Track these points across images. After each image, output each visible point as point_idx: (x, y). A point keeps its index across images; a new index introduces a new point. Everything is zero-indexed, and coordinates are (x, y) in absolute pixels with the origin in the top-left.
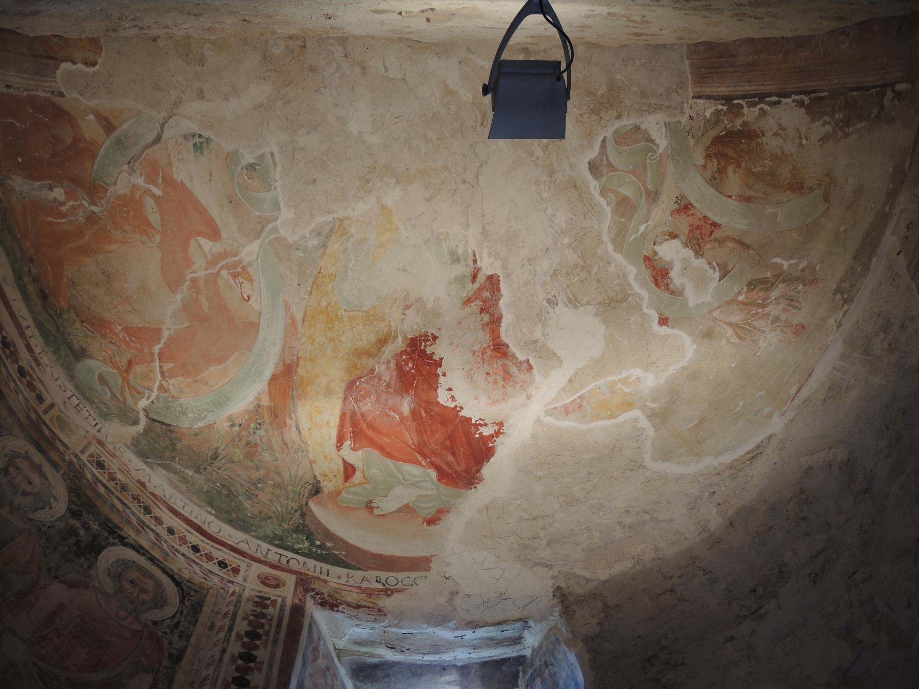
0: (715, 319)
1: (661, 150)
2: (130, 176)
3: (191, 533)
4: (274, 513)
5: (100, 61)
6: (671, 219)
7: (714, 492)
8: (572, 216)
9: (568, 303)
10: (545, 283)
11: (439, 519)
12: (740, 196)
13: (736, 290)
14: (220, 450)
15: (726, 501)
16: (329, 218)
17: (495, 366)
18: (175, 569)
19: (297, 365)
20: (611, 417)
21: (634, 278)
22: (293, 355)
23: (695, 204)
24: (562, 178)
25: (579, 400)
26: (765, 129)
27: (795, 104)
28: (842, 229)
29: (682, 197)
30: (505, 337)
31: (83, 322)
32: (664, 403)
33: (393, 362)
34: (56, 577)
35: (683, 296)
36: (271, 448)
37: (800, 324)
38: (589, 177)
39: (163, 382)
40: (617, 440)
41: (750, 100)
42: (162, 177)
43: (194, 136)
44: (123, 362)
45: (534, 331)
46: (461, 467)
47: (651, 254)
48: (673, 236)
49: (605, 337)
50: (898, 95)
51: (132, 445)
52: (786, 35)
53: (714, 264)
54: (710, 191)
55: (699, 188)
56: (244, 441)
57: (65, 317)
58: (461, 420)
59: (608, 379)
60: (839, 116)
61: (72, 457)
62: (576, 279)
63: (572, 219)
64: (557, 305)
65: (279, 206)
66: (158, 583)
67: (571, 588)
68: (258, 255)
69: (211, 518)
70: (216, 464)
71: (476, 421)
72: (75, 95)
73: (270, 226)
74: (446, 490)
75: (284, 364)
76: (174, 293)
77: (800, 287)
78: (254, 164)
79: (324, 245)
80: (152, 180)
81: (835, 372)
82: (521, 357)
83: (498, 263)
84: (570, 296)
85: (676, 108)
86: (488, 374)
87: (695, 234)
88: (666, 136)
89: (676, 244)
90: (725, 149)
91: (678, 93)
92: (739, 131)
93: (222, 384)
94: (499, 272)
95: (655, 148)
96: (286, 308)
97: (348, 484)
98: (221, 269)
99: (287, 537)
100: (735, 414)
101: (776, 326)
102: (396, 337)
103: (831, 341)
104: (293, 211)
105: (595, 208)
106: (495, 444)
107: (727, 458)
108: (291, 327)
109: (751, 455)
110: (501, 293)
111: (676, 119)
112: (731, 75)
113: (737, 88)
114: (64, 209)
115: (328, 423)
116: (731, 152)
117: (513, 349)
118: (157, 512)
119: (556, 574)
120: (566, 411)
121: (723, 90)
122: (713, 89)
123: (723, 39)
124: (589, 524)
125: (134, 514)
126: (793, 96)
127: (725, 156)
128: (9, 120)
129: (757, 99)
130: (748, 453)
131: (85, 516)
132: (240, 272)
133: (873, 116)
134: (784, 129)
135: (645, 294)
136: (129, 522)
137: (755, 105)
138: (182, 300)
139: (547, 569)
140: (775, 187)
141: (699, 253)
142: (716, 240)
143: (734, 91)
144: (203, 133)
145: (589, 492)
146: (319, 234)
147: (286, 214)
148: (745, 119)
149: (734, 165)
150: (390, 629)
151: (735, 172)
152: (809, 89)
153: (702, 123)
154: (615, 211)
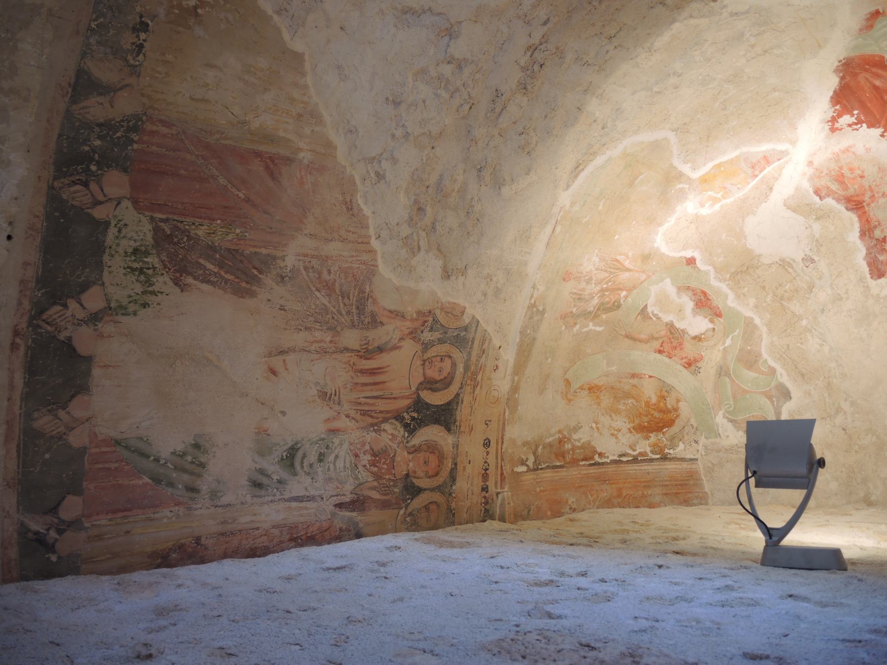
0: (643, 272)
1: (721, 413)
6: (702, 353)
7: (603, 128)
8: (802, 346)
9: (792, 262)
10: (820, 278)
11: (868, 20)
12: (642, 378)
13: (630, 299)
15: (590, 125)
17: (856, 187)
20: (719, 166)
21: (728, 296)
23: (682, 368)
24: (817, 382)
25: (757, 173)
26: (629, 434)
27: (606, 455)
28: (549, 360)
29: (695, 373)
30: (852, 220)
32: (671, 191)
35: (677, 286)
37: (568, 281)
38: (790, 385)
40: (707, 147)
41: (645, 458)
45: (822, 229)
46: (862, 78)
47: (715, 320)
48: (697, 338)
49: (745, 237)
50: (523, 463)
52: (619, 509)
53: (654, 319)
54: (670, 380)
55: (680, 382)
59: (732, 199)
60: (568, 446)
62: (787, 287)
63: (802, 344)
64: (803, 259)
67: (704, 4)
71: (862, 126)
77: (574, 310)
81: (528, 251)
82: (830, 201)
83: (875, 291)
84: (790, 270)
85: (712, 450)
86: (862, 177)
87: (676, 342)
88: (718, 426)
89: (693, 332)
90: (661, 417)
91: (712, 463)
92: (652, 432)
94: (872, 283)
95: (727, 415)
100: (604, 198)
101: (587, 276)
103: (537, 273)
105: (779, 357)
106: (833, 109)
107: (599, 160)
109: (581, 167)
110: (866, 262)
111: (710, 440)
112: (665, 478)
113: (658, 467)
116: (656, 414)
117: (841, 208)
119: (724, 11)
120: (767, 160)
121: (670, 466)
122: (680, 467)
123: (673, 508)
124: (709, 65)
126: (609, 462)
127: (661, 411)
129: (639, 458)
130: (583, 169)
133: (541, 447)
134: (612, 435)
135: (715, 283)
137: (641, 454)
139: (734, 11)
140: (612, 388)
141: (671, 327)
142: (657, 339)
143: (660, 465)
145: (719, 92)
148: (647, 442)
149: (651, 403)
151: (650, 398)
152: (596, 467)
153: (686, 438)
154: (758, 355)
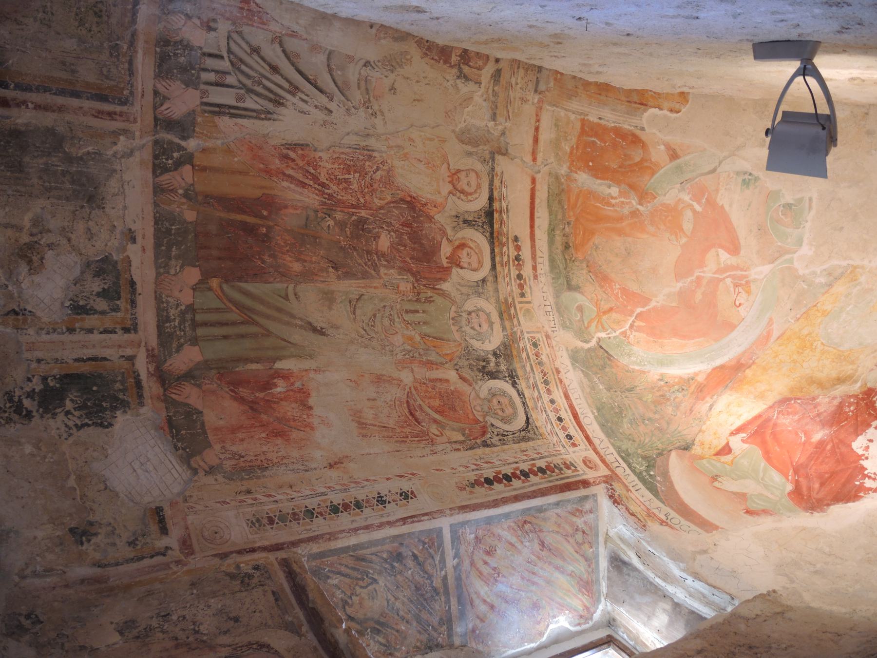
2: (679, 192)
3: (567, 412)
4: (640, 441)
5: (683, 110)
14: (638, 388)
16: (844, 263)
18: (534, 417)
19: (749, 367)
22: (751, 359)
31: (590, 272)
33: (839, 400)
34: (457, 370)
36: (677, 407)
39: (628, 331)
42: (706, 199)
43: (745, 173)
44: (605, 306)
51: (572, 351)
56: (661, 393)
57: (577, 263)
58: (856, 467)
61: (519, 331)
65: (802, 242)
66: (515, 414)
68: (765, 276)
69: (590, 415)
70: (627, 394)
72: (654, 131)
73: (787, 257)
74: (787, 502)
75: (738, 362)
76: (677, 281)
78: (791, 204)
79: (830, 285)
80: (697, 198)
93: (675, 352)
96: (769, 323)
97: (714, 458)
98: (727, 277)
99: (634, 457)
102: (856, 382)
104: (813, 249)
108: (764, 339)
114: (613, 201)
115: (740, 416)
118: (552, 387)
125: (534, 378)
128: (593, 139)
131: (501, 360)
132: (743, 284)
136: (528, 379)
138: (681, 288)
144: (753, 172)
146: (830, 274)
147: (806, 250)
150: (642, 541)
